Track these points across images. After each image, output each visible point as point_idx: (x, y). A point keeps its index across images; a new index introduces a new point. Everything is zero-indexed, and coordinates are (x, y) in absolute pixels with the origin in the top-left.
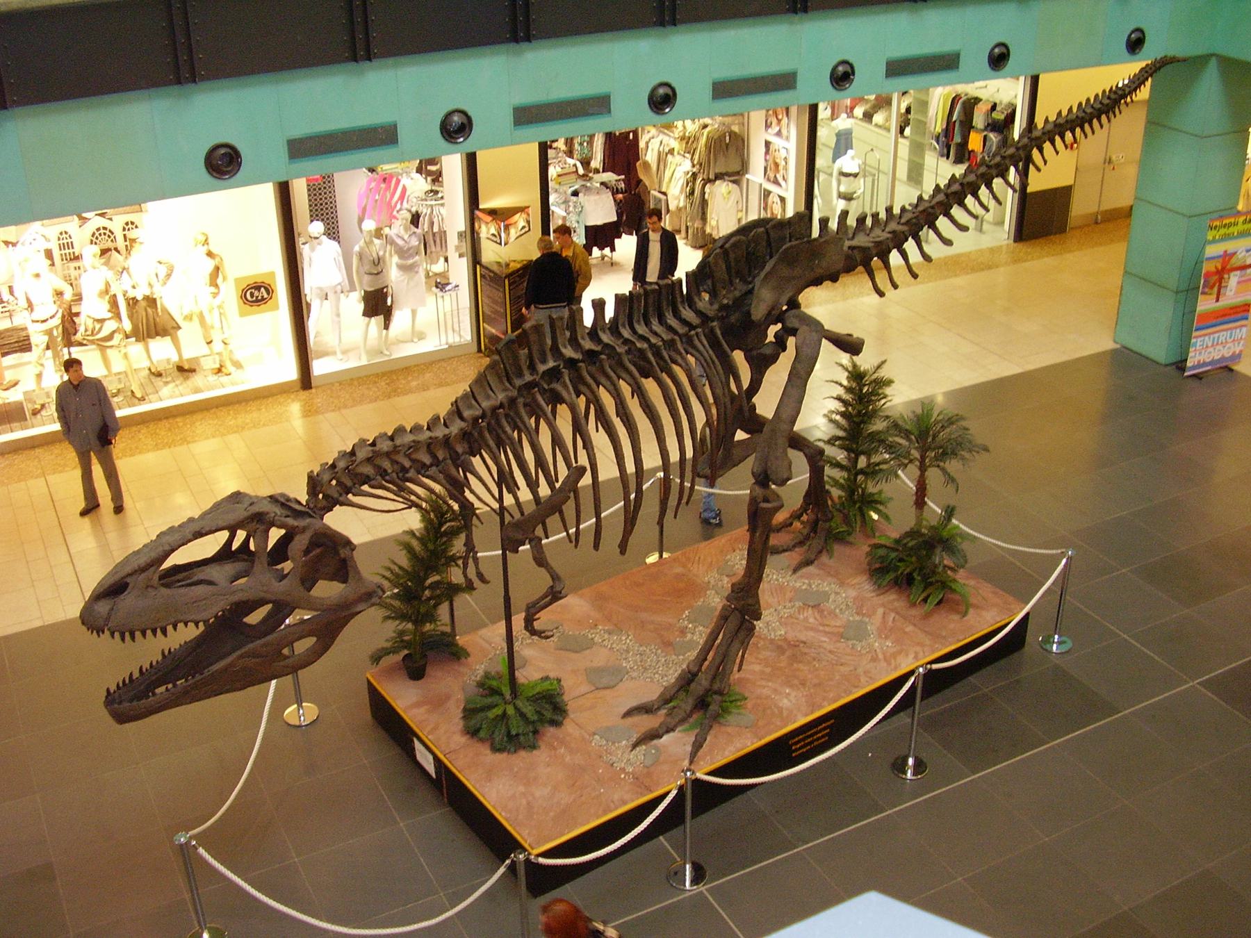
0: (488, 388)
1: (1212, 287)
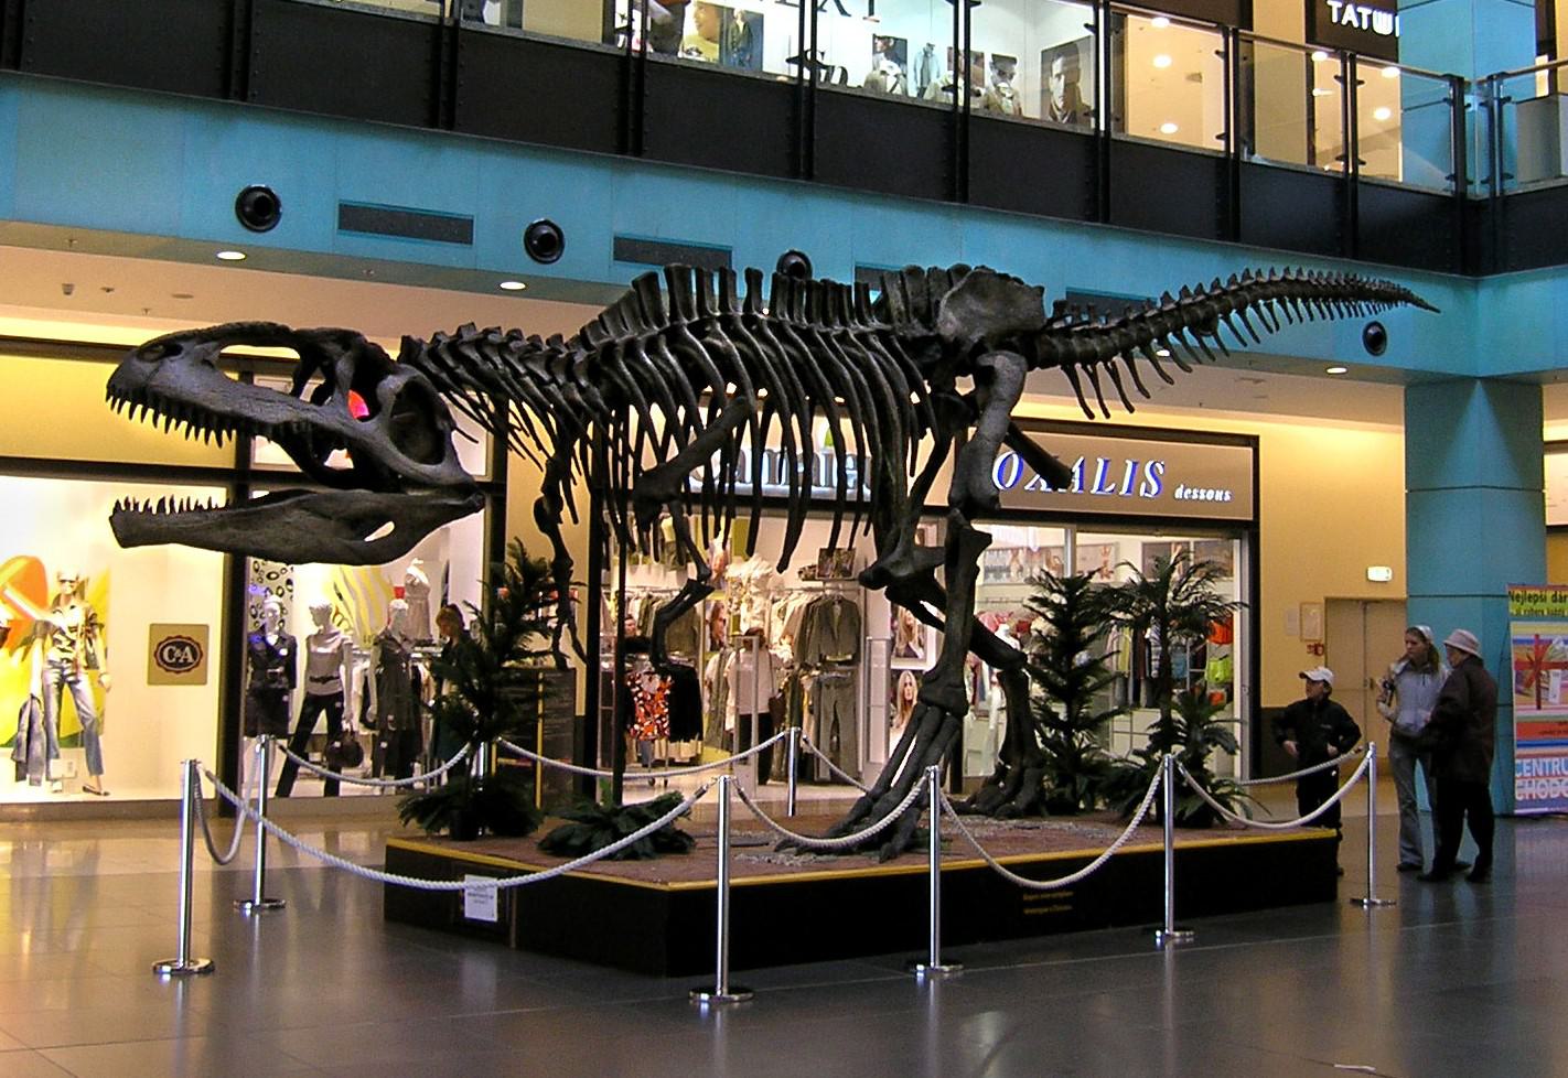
0: (621, 324)
1: (1528, 686)
